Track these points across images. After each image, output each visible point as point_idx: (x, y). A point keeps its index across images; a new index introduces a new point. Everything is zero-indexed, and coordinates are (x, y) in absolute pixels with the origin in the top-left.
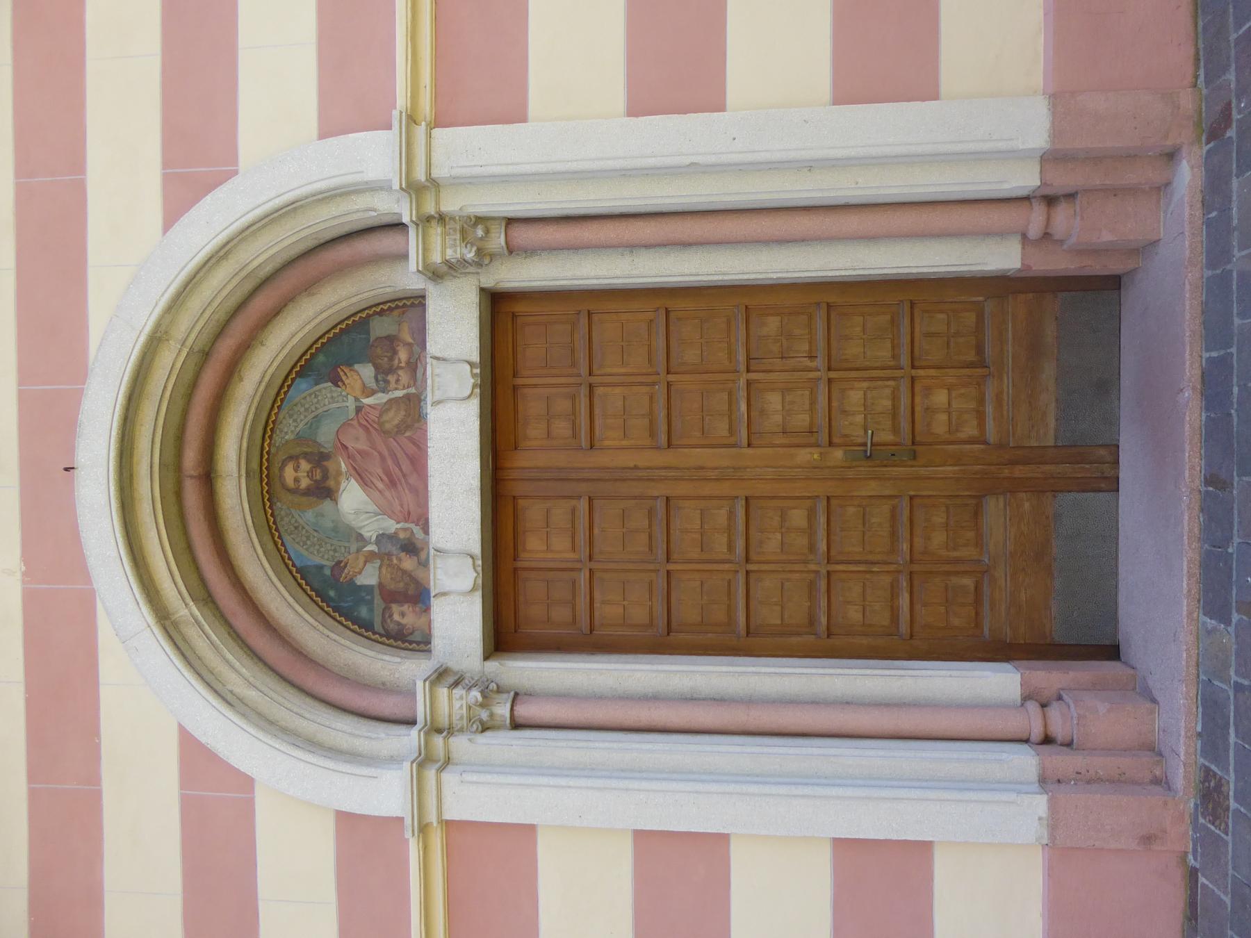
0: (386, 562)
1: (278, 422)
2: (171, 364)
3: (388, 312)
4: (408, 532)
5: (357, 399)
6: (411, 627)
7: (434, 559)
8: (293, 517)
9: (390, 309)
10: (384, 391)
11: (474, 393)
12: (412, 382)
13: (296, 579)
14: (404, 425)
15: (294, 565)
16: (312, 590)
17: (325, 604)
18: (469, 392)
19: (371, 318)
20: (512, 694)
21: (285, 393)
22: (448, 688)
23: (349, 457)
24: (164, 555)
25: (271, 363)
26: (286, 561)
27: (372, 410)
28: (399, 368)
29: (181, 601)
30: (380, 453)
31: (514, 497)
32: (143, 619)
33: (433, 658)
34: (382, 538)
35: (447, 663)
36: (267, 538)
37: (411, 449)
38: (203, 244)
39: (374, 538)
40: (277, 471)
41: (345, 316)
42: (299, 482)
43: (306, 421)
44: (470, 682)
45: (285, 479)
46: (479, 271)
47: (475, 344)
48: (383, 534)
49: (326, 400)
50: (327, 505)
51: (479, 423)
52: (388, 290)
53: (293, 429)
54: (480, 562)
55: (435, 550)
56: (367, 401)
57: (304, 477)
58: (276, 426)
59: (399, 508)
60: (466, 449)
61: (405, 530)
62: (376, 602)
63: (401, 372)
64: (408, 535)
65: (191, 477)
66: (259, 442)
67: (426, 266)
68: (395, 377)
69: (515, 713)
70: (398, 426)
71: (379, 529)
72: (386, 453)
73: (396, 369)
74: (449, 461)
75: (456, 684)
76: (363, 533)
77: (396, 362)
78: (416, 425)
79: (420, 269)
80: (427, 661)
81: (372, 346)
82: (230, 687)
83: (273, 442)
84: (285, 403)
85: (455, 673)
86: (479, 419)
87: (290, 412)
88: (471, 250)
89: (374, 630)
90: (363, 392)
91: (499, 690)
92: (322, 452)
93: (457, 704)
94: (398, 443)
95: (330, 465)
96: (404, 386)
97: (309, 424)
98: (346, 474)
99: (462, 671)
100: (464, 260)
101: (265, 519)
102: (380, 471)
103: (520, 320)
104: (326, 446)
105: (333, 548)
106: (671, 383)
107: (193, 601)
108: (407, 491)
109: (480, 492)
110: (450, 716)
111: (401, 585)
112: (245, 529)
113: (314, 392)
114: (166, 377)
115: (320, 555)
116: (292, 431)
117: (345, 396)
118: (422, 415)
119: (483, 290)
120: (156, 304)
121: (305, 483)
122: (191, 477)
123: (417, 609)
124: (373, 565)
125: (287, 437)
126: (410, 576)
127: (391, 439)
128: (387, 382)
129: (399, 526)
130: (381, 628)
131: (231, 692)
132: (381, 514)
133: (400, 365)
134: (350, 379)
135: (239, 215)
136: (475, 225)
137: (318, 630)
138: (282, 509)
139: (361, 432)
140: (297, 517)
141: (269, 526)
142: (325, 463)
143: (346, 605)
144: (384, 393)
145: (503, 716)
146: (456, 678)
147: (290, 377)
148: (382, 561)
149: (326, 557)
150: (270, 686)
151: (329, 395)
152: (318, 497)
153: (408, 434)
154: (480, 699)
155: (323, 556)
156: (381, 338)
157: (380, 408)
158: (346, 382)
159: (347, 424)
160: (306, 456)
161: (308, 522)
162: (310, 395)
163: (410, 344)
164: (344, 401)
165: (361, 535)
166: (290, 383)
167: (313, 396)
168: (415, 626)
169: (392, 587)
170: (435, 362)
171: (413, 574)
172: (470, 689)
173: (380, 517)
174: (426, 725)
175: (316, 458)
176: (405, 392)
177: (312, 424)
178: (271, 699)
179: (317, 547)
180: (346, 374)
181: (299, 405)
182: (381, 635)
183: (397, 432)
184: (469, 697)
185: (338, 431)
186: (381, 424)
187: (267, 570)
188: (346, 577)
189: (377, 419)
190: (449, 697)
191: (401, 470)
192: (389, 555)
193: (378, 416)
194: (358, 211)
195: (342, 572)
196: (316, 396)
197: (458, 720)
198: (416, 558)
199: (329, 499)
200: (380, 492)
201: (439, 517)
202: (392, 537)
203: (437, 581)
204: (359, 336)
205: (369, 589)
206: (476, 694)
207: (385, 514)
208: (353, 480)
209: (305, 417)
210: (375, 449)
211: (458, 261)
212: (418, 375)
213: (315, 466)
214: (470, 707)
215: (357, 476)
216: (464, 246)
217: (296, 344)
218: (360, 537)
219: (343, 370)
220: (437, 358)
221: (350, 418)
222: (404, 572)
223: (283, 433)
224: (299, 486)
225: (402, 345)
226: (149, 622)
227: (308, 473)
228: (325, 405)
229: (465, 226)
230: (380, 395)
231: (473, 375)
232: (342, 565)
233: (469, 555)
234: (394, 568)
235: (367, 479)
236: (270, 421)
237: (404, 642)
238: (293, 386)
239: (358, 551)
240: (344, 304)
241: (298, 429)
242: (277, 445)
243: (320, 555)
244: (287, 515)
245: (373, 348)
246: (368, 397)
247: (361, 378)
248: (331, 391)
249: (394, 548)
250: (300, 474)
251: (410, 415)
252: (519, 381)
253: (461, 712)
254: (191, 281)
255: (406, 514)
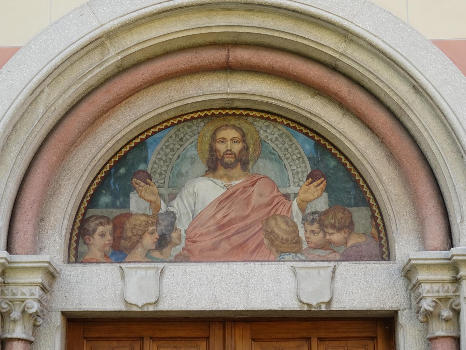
0: (150, 220)
1: (275, 124)
2: (325, 44)
3: (374, 223)
4: (177, 240)
5: (296, 195)
6: (91, 242)
7: (154, 268)
8: (191, 137)
9: (377, 226)
10: (304, 220)
11: (303, 305)
12: (312, 245)
13: (134, 139)
14: (273, 238)
15: (148, 137)
16: (126, 153)
17: (113, 164)
18: (304, 300)
19: (369, 208)
20: (32, 339)
21: (301, 131)
22: (41, 283)
23: (245, 187)
24: (161, 36)
25: (328, 123)
26: (152, 130)
27: (287, 209)
28: (325, 233)
29: (121, 49)
30: (248, 216)
31: (208, 338)
32: (108, 20)
33: (65, 265)
34: (172, 216)
35: (60, 277)
36: (173, 114)
37: (252, 245)
38: (427, 76)
39: (171, 209)
40: (232, 123)
41: (370, 185)
42: (222, 142)
43: (277, 149)
44: (43, 300)
45: (225, 130)
46: (413, 310)
47: (348, 307)
48: (175, 217)
49: (295, 168)
50: (201, 167)
51: (277, 309)
52: (394, 227)
53: (269, 138)
54: (151, 309)
55: (163, 269)
56: (295, 204)
57: (227, 147)
58: (272, 122)
59: (199, 233)
60: (253, 297)
61: (179, 238)
62: (114, 210)
63: (321, 235)
64: (175, 240)
65: (228, 56)
66: (258, 107)
67: (414, 267)
68: (317, 230)
69: (15, 343)
70: (272, 232)
71: (180, 214)
72: (248, 221)
73: (324, 231)
74: (242, 282)
75: (43, 288)
76: (176, 199)
77: (331, 231)
78: (274, 249)
79: (412, 262)
80: (62, 260)
81: (344, 209)
82: (46, 90)
83: (258, 119)
84: (292, 130)
85: (50, 285)
86: (280, 309)
87: (284, 135)
88: (430, 306)
89: (89, 208)
90: (303, 201)
91: (35, 326)
92: (248, 163)
93: (26, 290)
94: (258, 231)
95: (238, 170)
96: (308, 238)
97: (274, 152)
98: (229, 185)
99: (52, 292)
100: (421, 299)
101: (189, 112)
102: (232, 215)
103: (370, 343)
104: (254, 167)
105: (163, 172)
106: (309, 341)
107: (122, 59)
108: (214, 240)
109: (215, 309)
110: (16, 284)
111: (129, 234)
112: (182, 98)
113: (302, 157)
114: (314, 40)
115: (157, 161)
116: (267, 137)
117: (299, 184)
118: (282, 254)
119: (396, 312)
120: (376, 36)
121: (221, 148)
122: (228, 56)
123: (107, 249)
124: (148, 209)
125: (262, 132)
126: (138, 242)
127: (261, 226)
128: (312, 222)
129: (183, 232)
130: (91, 215)
131: (42, 91)
132: (193, 216)
133: (328, 234)
134: (315, 189)
135: (453, 107)
136: (453, 310)
137: (91, 161)
138: (198, 127)
139: (266, 200)
140: (191, 140)
141: (183, 115)
142: (239, 166)
143: (112, 184)
144: (302, 219)
145: (14, 330)
146: (48, 287)
147: (315, 135)
148: (152, 217)
149: (156, 166)
150: (46, 123)
151: (299, 170)
152: (209, 159)
153: (266, 241)
154: (31, 311)
155: (156, 163)
156: (351, 217)
157: (289, 216)
158: (312, 186)
159: (274, 186)
160: (246, 148)
161: (186, 149)
162: (299, 153)
163: (346, 243)
164: (295, 183)
165: (174, 198)
166: (310, 135)
167: (299, 156)
168: (92, 246)
169: (128, 226)
170: (331, 269)
171: (139, 244)
172: (39, 301)
173: (191, 215)
174: (9, 263)
175: (243, 158)
176: (304, 239)
177: (274, 154)
178: (35, 126)
179: (164, 158)
180: (318, 185)
181: (290, 143)
182: (84, 215)
183: (268, 231)
184: (32, 301)
185: (268, 178)
186: (274, 217)
187: (145, 116)
188: (137, 184)
189: (279, 213)
190: (34, 283)
191: (233, 235)
192: (157, 223)
193: (282, 214)
194: (461, 207)
195: (141, 180)
196: (298, 158)
197: (12, 290)
198: (154, 247)
199: (207, 169)
200: (214, 215)
201: (193, 272)
202: (172, 226)
203: (134, 270)
204: (353, 197)
205: (126, 204)
206: (34, 307)
207: (193, 220)
208: (224, 191)
209: (280, 149)
210: (252, 211)
211: (420, 294)
212: (321, 250)
213: (237, 156)
214: (23, 302)
215: (228, 194)
216: (434, 300)
217: (344, 144)
218: (173, 197)
219: (322, 183)
220: (334, 272)
221: (280, 189)
222: (141, 237)
223: (266, 128)
224: (219, 142)
225: (346, 236)
226: (105, 26)
227: (230, 150)
228: (291, 166)
229: (451, 301)
230: (301, 216)
231: (319, 305)
232: (148, 180)
233: (158, 299)
234: (145, 227)
235: (225, 204)
236: (276, 117)
237: (78, 235)
238: (308, 138)
239: (161, 195)
240: (380, 187)
241: (269, 142)
242: (255, 123)
243: (157, 161)
244: (192, 131)
245: (342, 210)
246: (298, 205)
247: (315, 199)
248: (303, 172)
249: (163, 228)
250: (229, 143)
251: (283, 243)
252: (314, 343)
253: (19, 294)
254: (397, 64)
255: (194, 239)
